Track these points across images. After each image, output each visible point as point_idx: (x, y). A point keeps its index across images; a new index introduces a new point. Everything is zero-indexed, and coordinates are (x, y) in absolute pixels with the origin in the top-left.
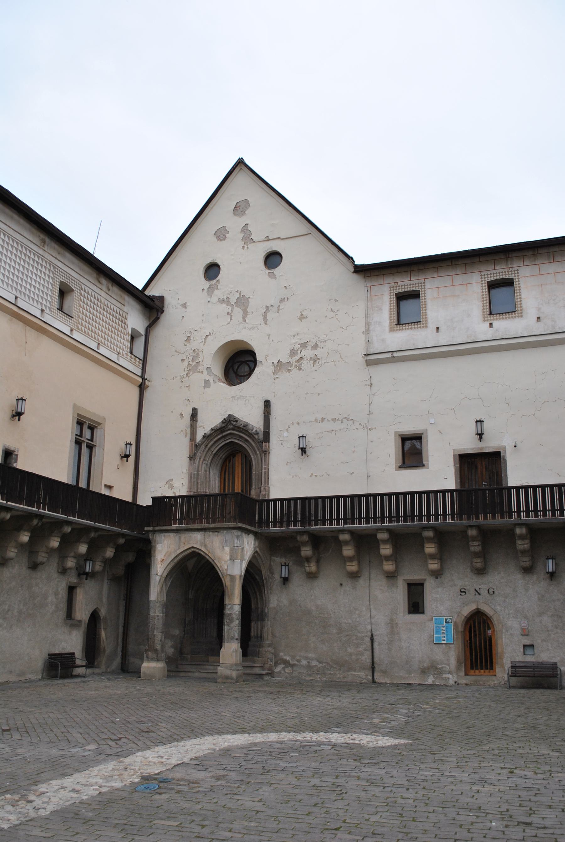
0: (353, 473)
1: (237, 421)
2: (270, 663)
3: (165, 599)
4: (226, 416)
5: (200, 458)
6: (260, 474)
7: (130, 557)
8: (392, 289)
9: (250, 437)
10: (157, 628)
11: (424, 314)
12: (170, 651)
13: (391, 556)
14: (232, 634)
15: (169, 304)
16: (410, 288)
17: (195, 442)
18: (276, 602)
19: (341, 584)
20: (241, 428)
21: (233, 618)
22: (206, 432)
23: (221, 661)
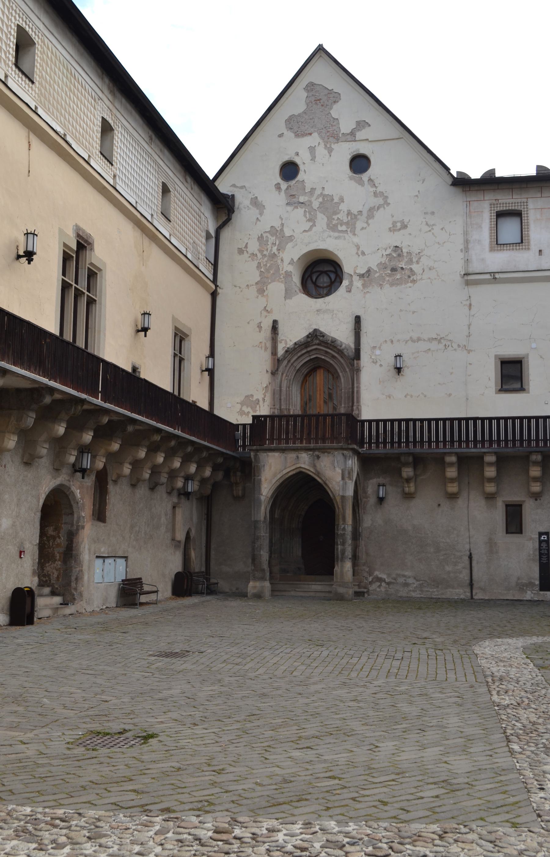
0: (450, 395)
1: (323, 336)
2: (365, 581)
4: (311, 330)
8: (493, 206)
9: (338, 353)
11: (526, 235)
13: (495, 478)
15: (240, 203)
16: (512, 206)
19: (439, 505)
20: (328, 343)
22: (288, 346)
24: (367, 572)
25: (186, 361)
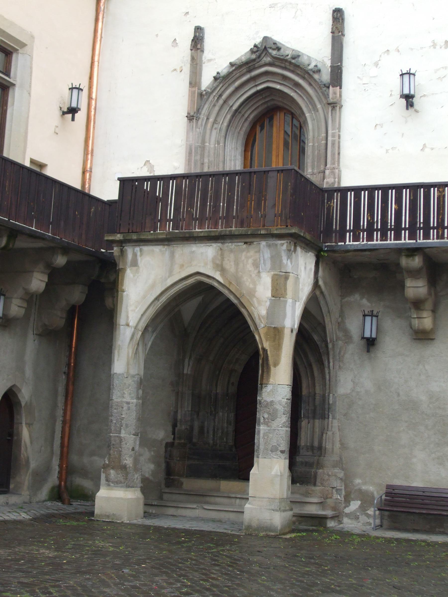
1: (279, 49)
2: (336, 496)
3: (142, 373)
5: (208, 119)
6: (323, 147)
7: (77, 295)
9: (303, 78)
10: (127, 426)
12: (148, 468)
14: (274, 443)
17: (199, 88)
18: (350, 385)
20: (286, 61)
21: (276, 411)
23: (251, 492)
24: (341, 479)
25: (17, 89)
